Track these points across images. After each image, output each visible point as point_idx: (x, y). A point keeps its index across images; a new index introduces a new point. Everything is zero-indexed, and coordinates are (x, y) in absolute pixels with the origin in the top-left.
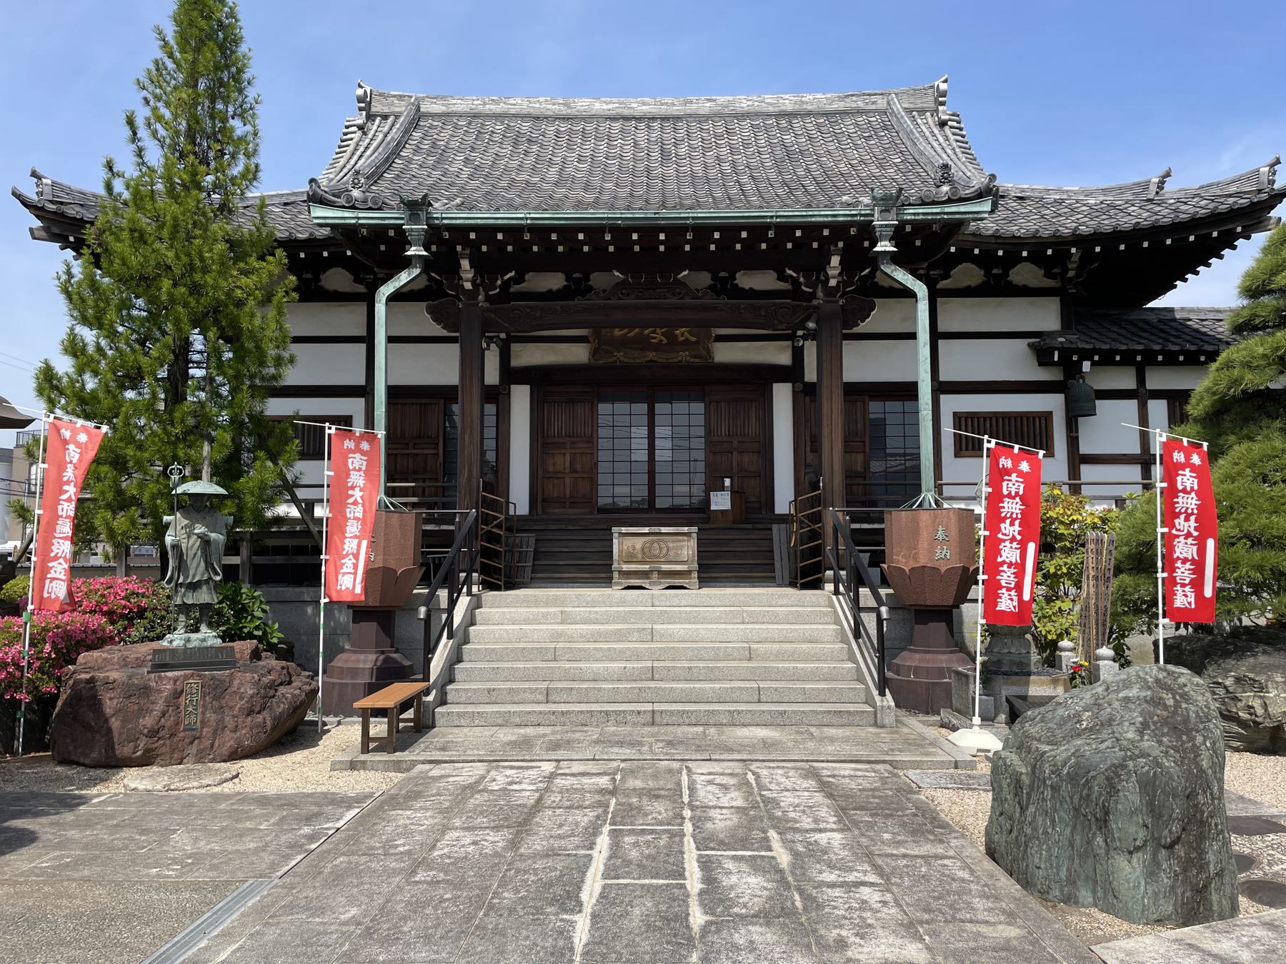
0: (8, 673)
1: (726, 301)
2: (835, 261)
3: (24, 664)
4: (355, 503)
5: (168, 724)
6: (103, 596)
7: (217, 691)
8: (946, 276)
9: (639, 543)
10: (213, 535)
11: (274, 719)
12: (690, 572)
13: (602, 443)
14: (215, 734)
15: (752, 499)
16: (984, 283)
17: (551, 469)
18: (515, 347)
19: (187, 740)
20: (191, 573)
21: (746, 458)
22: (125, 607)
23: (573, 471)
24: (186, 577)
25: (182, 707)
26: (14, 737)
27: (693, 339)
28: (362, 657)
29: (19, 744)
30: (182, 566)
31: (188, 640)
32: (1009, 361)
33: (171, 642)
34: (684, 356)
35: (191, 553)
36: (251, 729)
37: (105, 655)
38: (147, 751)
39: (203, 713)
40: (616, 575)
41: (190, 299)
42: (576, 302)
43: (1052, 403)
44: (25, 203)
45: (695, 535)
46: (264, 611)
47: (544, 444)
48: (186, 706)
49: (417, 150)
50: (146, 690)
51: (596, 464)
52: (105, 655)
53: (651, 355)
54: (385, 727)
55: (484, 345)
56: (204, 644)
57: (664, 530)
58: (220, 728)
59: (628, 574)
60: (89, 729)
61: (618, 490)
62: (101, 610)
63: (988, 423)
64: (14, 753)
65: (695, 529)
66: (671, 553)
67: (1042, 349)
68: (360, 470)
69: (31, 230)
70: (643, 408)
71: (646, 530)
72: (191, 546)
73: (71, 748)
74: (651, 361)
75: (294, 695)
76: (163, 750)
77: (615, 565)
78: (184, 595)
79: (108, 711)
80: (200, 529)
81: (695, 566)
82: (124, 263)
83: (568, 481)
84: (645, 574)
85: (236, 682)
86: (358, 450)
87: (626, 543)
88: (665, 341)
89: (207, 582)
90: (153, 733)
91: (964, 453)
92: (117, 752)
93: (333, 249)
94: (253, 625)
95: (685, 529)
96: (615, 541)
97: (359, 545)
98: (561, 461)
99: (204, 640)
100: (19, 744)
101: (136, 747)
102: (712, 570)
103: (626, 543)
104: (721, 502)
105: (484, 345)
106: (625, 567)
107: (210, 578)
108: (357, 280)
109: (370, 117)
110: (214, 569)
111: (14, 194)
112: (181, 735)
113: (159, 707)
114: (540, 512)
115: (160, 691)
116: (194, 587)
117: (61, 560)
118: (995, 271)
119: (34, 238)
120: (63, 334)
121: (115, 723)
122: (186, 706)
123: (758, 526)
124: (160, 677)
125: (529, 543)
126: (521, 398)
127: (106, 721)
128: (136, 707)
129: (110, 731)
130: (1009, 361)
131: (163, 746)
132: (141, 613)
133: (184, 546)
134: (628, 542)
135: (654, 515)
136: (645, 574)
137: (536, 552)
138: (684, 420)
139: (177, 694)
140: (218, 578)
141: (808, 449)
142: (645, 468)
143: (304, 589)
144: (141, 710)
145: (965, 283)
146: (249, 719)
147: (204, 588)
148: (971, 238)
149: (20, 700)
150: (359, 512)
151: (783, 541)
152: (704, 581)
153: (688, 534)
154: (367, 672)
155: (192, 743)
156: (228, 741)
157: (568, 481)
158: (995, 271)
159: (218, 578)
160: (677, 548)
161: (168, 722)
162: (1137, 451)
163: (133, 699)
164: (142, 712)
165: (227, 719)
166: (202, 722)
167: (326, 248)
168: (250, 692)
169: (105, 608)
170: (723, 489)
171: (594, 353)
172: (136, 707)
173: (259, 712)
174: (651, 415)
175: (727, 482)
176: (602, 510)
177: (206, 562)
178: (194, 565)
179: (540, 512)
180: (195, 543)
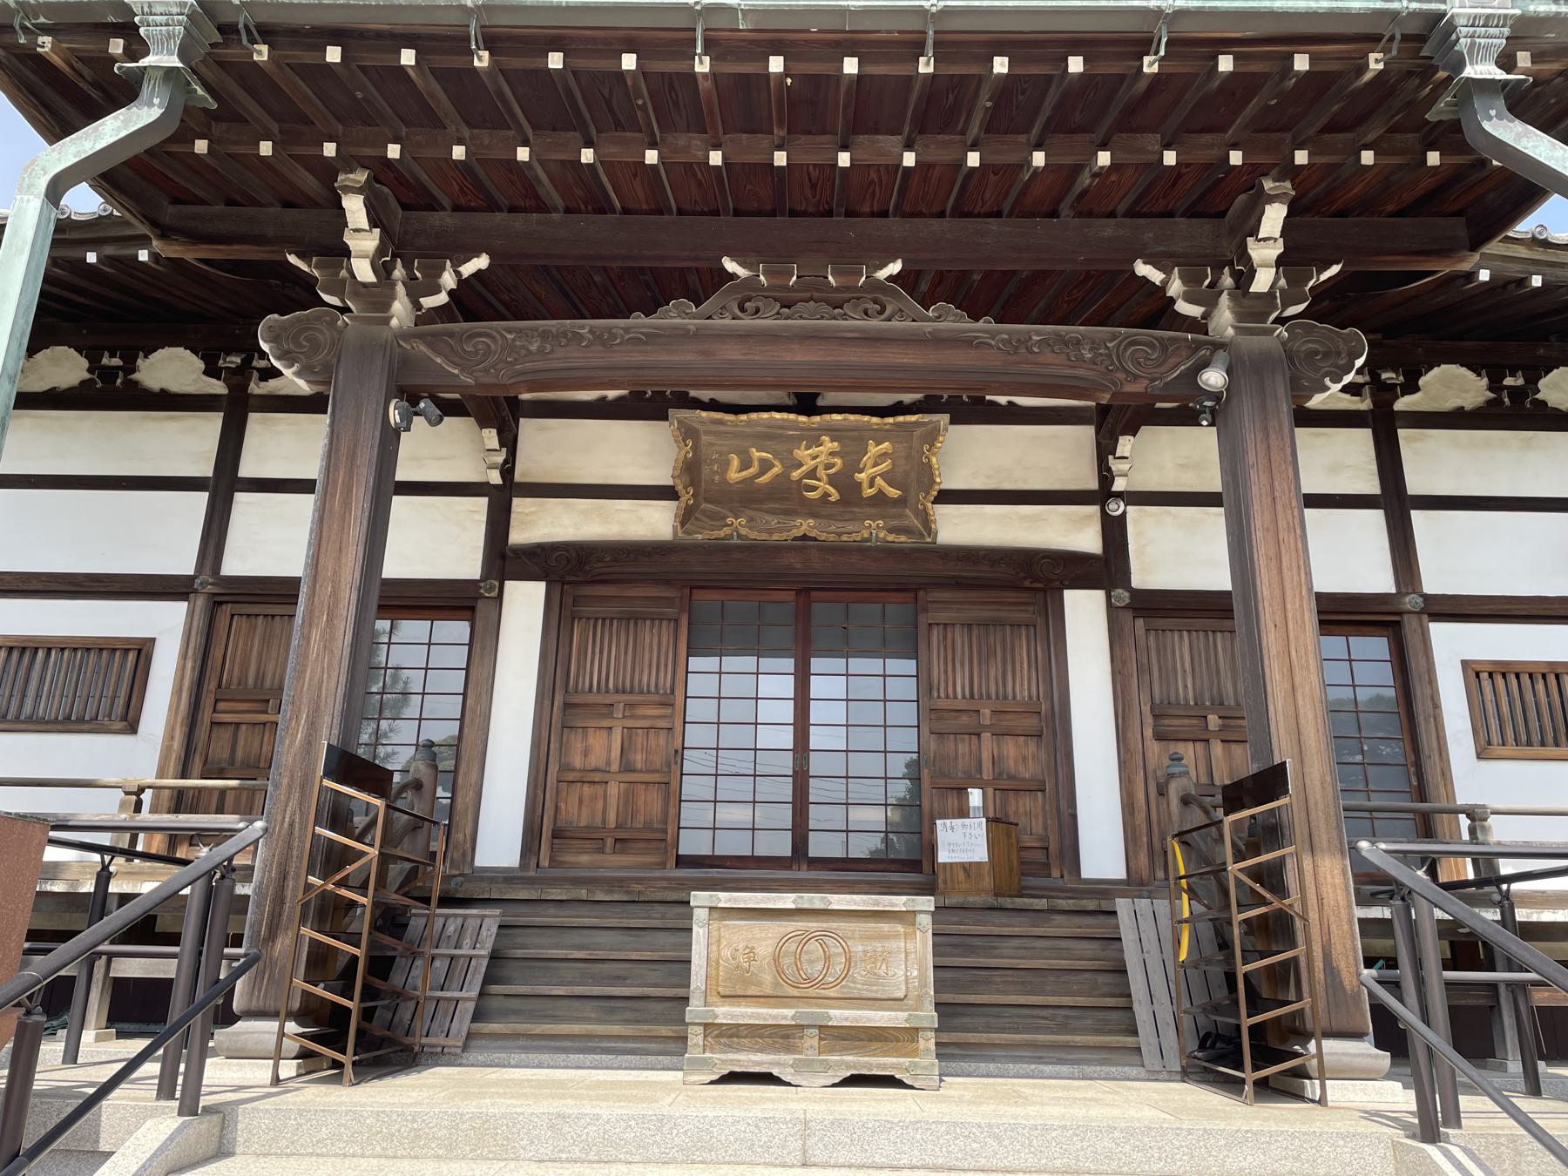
1: (994, 326)
2: (1274, 218)
8: (1411, 387)
9: (765, 937)
12: (912, 1033)
13: (695, 710)
15: (1028, 841)
16: (1489, 402)
17: (577, 762)
18: (520, 505)
21: (1011, 748)
23: (627, 767)
27: (894, 493)
34: (874, 530)
40: (696, 1036)
42: (630, 321)
45: (925, 921)
47: (567, 706)
51: (679, 753)
53: (805, 525)
55: (394, 416)
57: (839, 901)
59: (731, 1034)
61: (728, 814)
63: (1540, 686)
65: (926, 903)
66: (858, 973)
71: (787, 900)
74: (804, 537)
77: (695, 1009)
81: (928, 1015)
83: (613, 790)
84: (783, 1037)
87: (726, 939)
88: (835, 495)
91: (1498, 750)
93: (110, 250)
95: (899, 902)
96: (699, 933)
98: (600, 746)
105: (394, 416)
106: (726, 1013)
114: (545, 862)
118: (1509, 381)
123: (1063, 904)
125: (479, 931)
126: (525, 603)
134: (739, 934)
135: (804, 874)
136: (783, 1037)
137: (495, 957)
138: (873, 688)
141: (1149, 732)
142: (786, 763)
145: (1449, 403)
148: (1523, 252)
153: (907, 917)
157: (613, 790)
158: (1509, 381)
160: (874, 958)
167: (93, 244)
170: (963, 812)
171: (686, 517)
175: (975, 797)
176: (683, 861)
179: (545, 862)
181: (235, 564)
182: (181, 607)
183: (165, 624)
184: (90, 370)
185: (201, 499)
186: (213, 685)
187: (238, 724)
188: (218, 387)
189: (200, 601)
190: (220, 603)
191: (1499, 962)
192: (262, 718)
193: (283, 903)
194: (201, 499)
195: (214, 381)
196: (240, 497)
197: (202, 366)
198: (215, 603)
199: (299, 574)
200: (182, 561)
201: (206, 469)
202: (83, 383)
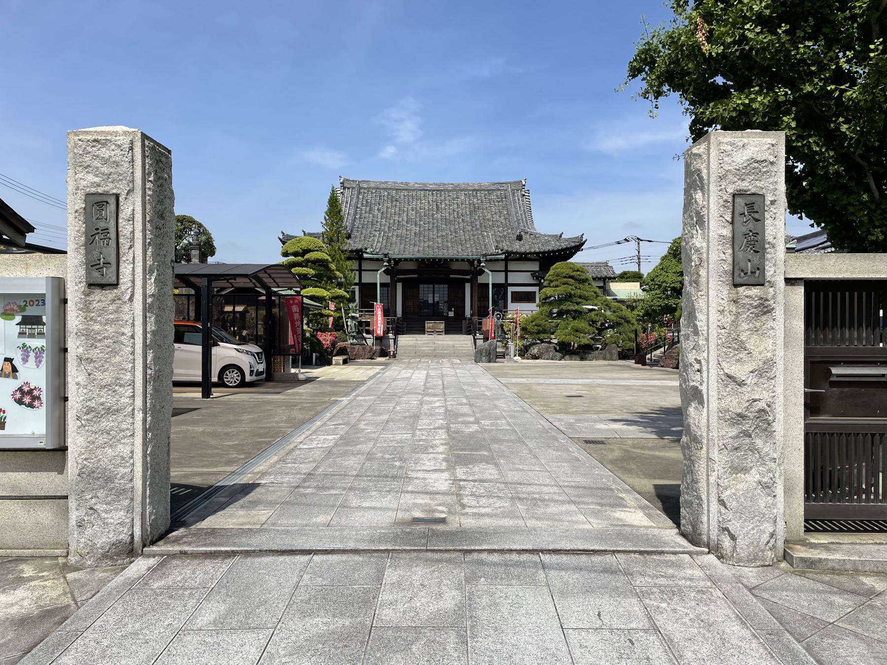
32: (526, 278)
43: (535, 289)
49: (362, 204)
54: (172, 474)
67: (534, 274)
70: (431, 286)
87: (428, 325)
102: (448, 331)
103: (428, 325)
104: (451, 314)
109: (344, 188)
126: (399, 286)
130: (526, 278)
151: (464, 324)
152: (446, 334)
162: (200, 379)
174: (434, 288)
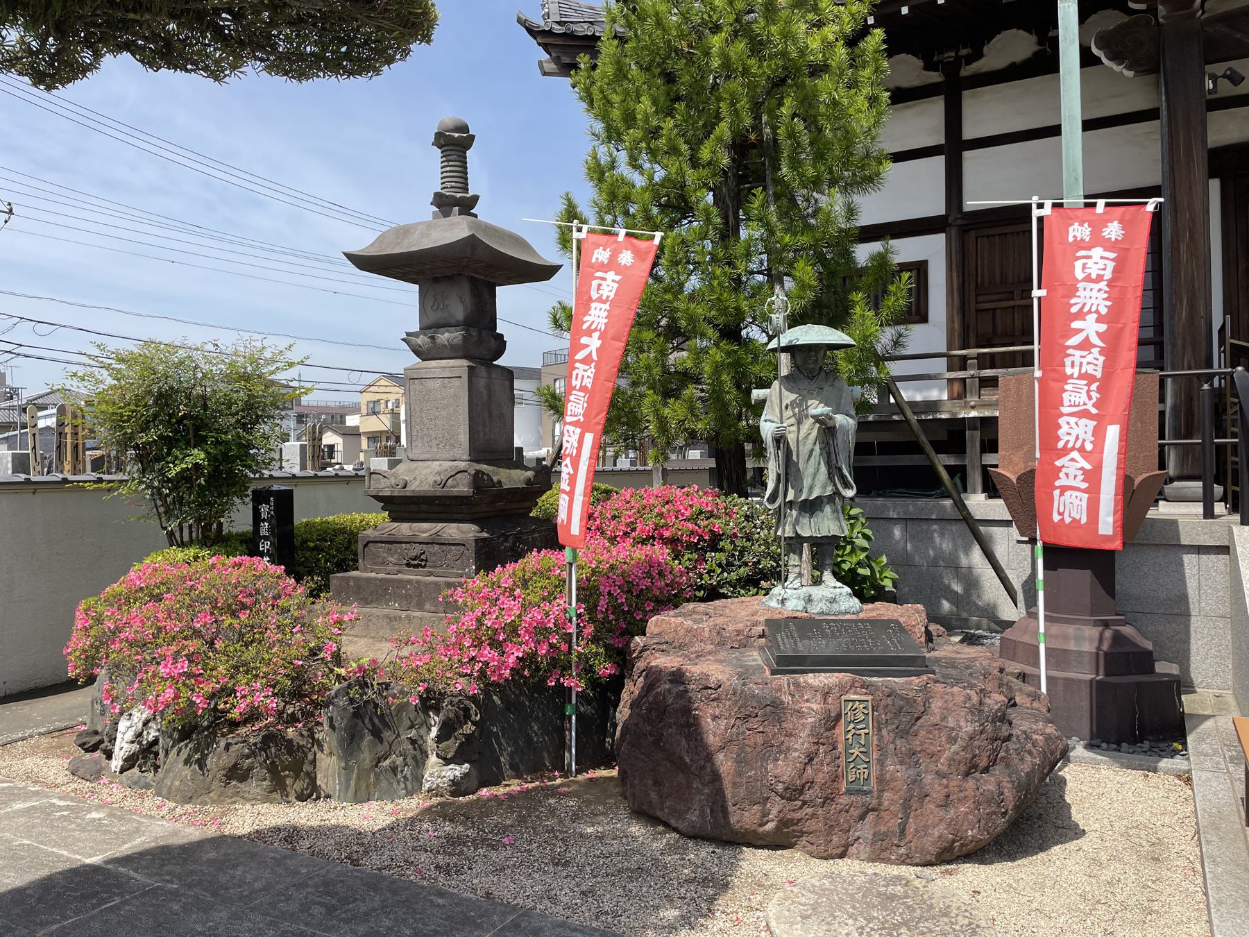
0: (551, 646)
3: (573, 630)
4: (1086, 345)
5: (820, 778)
6: (661, 515)
7: (903, 718)
8: (978, 55)
10: (840, 419)
11: (1019, 787)
14: (906, 806)
19: (856, 812)
20: (807, 482)
22: (692, 533)
24: (799, 491)
25: (841, 748)
26: (562, 746)
28: (1071, 629)
29: (570, 757)
30: (790, 472)
31: (809, 600)
33: (783, 601)
35: (804, 450)
36: (978, 803)
37: (688, 623)
38: (784, 823)
39: (881, 762)
41: (752, 61)
44: (533, 32)
46: (865, 536)
48: (849, 746)
50: (775, 710)
52: (688, 623)
56: (835, 607)
58: (914, 798)
60: (682, 767)
62: (661, 537)
64: (566, 773)
68: (1100, 278)
69: (540, 63)
72: (805, 437)
73: (653, 795)
75: (1048, 738)
76: (812, 825)
78: (797, 522)
79: (712, 740)
80: (817, 408)
82: (659, 23)
85: (936, 704)
86: (1097, 240)
89: (831, 499)
90: (794, 792)
92: (733, 819)
94: (854, 560)
97: (1099, 434)
99: (833, 601)
100: (570, 757)
101: (765, 814)
107: (837, 493)
108: (929, 67)
110: (842, 477)
111: (519, 21)
112: (844, 800)
113: (801, 744)
115: (800, 714)
116: (811, 507)
117: (1075, 455)
119: (545, 74)
120: (584, 156)
121: (725, 763)
122: (849, 746)
124: (797, 685)
127: (709, 758)
128: (760, 739)
129: (716, 777)
131: (811, 818)
132: (714, 542)
133: (791, 438)
139: (832, 721)
140: (850, 493)
143: (889, 502)
144: (768, 745)
146: (971, 784)
147: (828, 509)
149: (570, 689)
150: (1093, 362)
154: (1086, 659)
155: (862, 817)
156: (935, 827)
159: (850, 493)
161: (821, 774)
163: (754, 723)
164: (771, 749)
165: (928, 778)
166: (881, 779)
168: (969, 728)
169: (667, 534)
172: (760, 739)
173: (986, 770)
177: (829, 464)
178: (811, 470)
180: (809, 430)
181: (972, 203)
182: (941, 238)
183: (931, 250)
184: (1039, 43)
185: (939, 162)
186: (973, 286)
187: (994, 310)
188: (935, 77)
189: (954, 231)
190: (967, 231)
191: (1229, 434)
192: (1011, 303)
193: (1193, 415)
194: (939, 162)
195: (932, 73)
196: (967, 155)
197: (920, 63)
198: (964, 231)
199: (1160, 183)
200: (935, 206)
201: (939, 139)
202: (1035, 54)
